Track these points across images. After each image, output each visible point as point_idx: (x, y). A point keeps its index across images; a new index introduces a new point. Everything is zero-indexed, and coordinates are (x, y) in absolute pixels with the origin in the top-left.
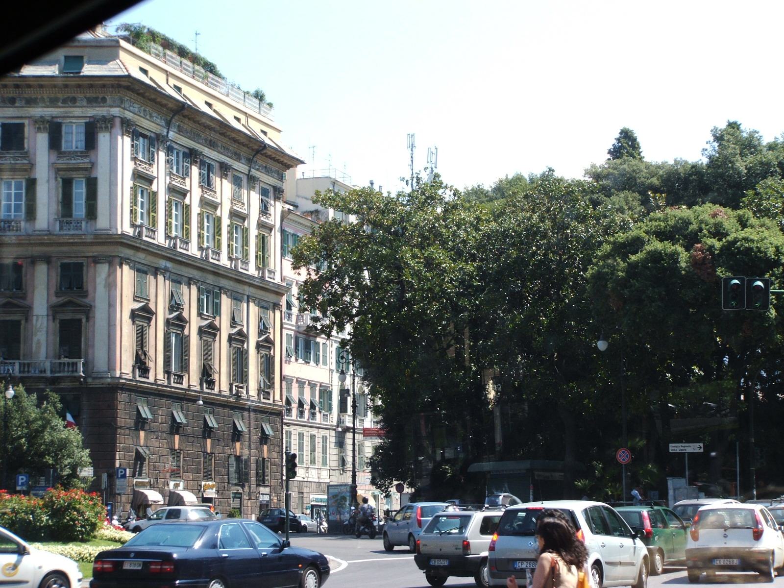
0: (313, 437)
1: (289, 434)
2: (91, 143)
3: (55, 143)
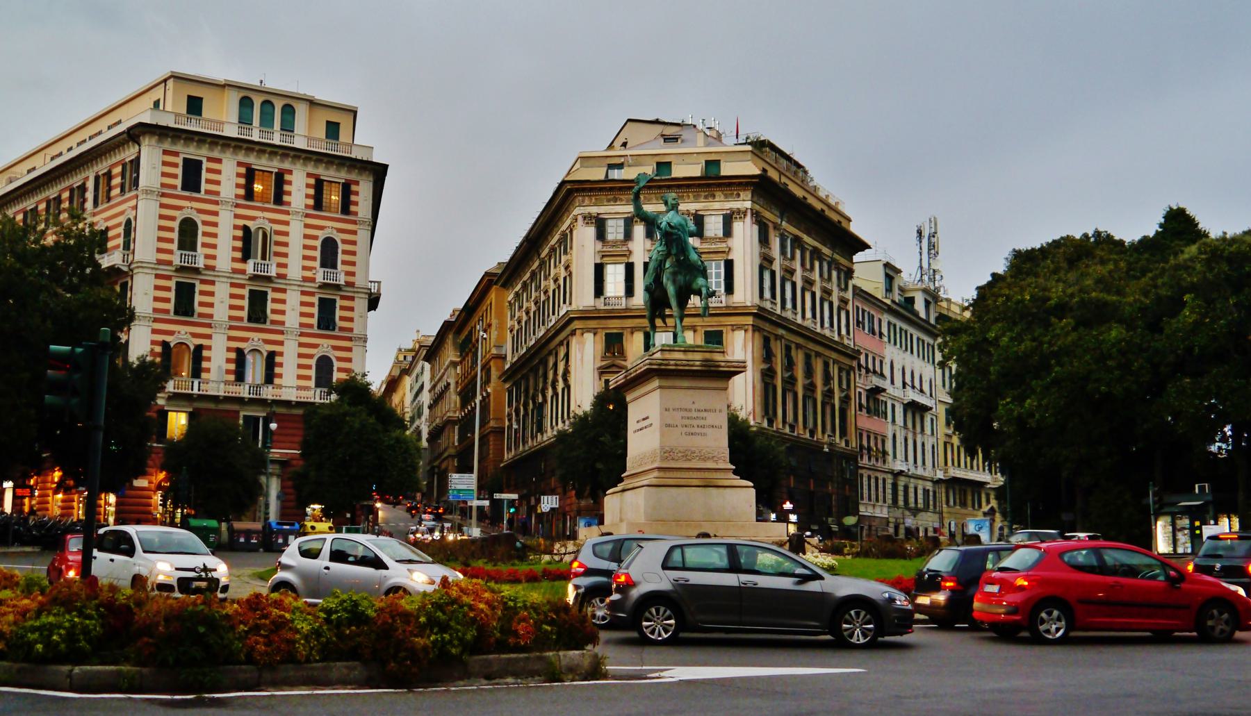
0: (877, 479)
1: (862, 476)
2: (728, 232)
3: (601, 235)
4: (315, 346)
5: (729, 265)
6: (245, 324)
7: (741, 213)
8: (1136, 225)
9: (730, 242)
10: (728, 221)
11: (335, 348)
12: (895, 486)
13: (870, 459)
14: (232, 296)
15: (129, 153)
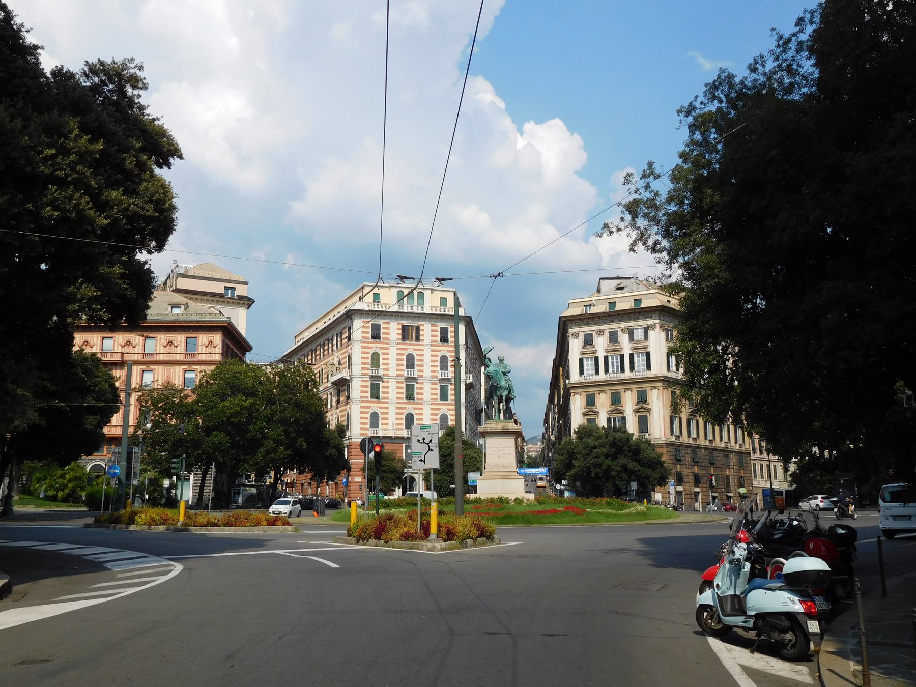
1: (754, 465)
2: (646, 337)
3: (631, 339)
4: (439, 409)
5: (648, 355)
6: (439, 401)
7: (654, 326)
8: (30, 39)
9: (647, 343)
10: (646, 330)
11: (415, 409)
12: (769, 467)
13: (761, 454)
14: (398, 388)
15: (347, 323)
